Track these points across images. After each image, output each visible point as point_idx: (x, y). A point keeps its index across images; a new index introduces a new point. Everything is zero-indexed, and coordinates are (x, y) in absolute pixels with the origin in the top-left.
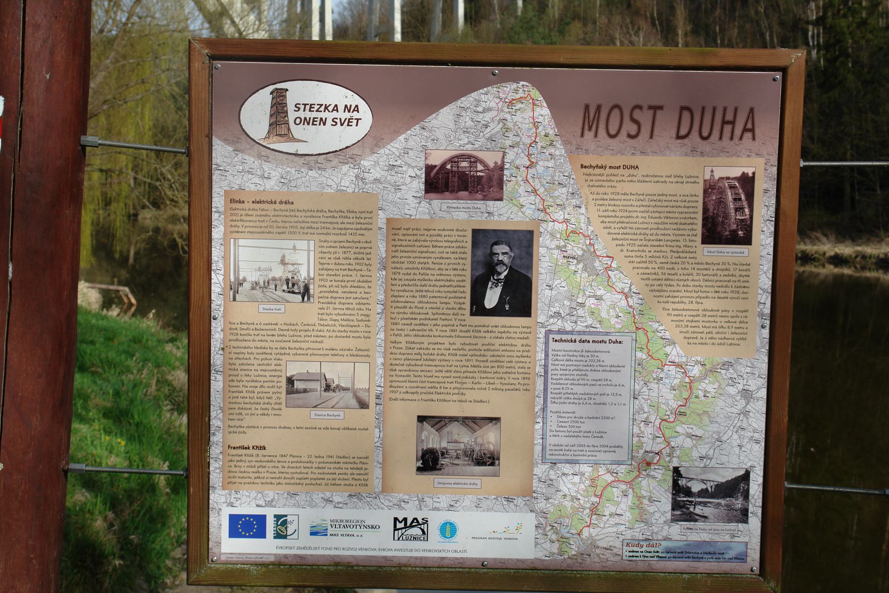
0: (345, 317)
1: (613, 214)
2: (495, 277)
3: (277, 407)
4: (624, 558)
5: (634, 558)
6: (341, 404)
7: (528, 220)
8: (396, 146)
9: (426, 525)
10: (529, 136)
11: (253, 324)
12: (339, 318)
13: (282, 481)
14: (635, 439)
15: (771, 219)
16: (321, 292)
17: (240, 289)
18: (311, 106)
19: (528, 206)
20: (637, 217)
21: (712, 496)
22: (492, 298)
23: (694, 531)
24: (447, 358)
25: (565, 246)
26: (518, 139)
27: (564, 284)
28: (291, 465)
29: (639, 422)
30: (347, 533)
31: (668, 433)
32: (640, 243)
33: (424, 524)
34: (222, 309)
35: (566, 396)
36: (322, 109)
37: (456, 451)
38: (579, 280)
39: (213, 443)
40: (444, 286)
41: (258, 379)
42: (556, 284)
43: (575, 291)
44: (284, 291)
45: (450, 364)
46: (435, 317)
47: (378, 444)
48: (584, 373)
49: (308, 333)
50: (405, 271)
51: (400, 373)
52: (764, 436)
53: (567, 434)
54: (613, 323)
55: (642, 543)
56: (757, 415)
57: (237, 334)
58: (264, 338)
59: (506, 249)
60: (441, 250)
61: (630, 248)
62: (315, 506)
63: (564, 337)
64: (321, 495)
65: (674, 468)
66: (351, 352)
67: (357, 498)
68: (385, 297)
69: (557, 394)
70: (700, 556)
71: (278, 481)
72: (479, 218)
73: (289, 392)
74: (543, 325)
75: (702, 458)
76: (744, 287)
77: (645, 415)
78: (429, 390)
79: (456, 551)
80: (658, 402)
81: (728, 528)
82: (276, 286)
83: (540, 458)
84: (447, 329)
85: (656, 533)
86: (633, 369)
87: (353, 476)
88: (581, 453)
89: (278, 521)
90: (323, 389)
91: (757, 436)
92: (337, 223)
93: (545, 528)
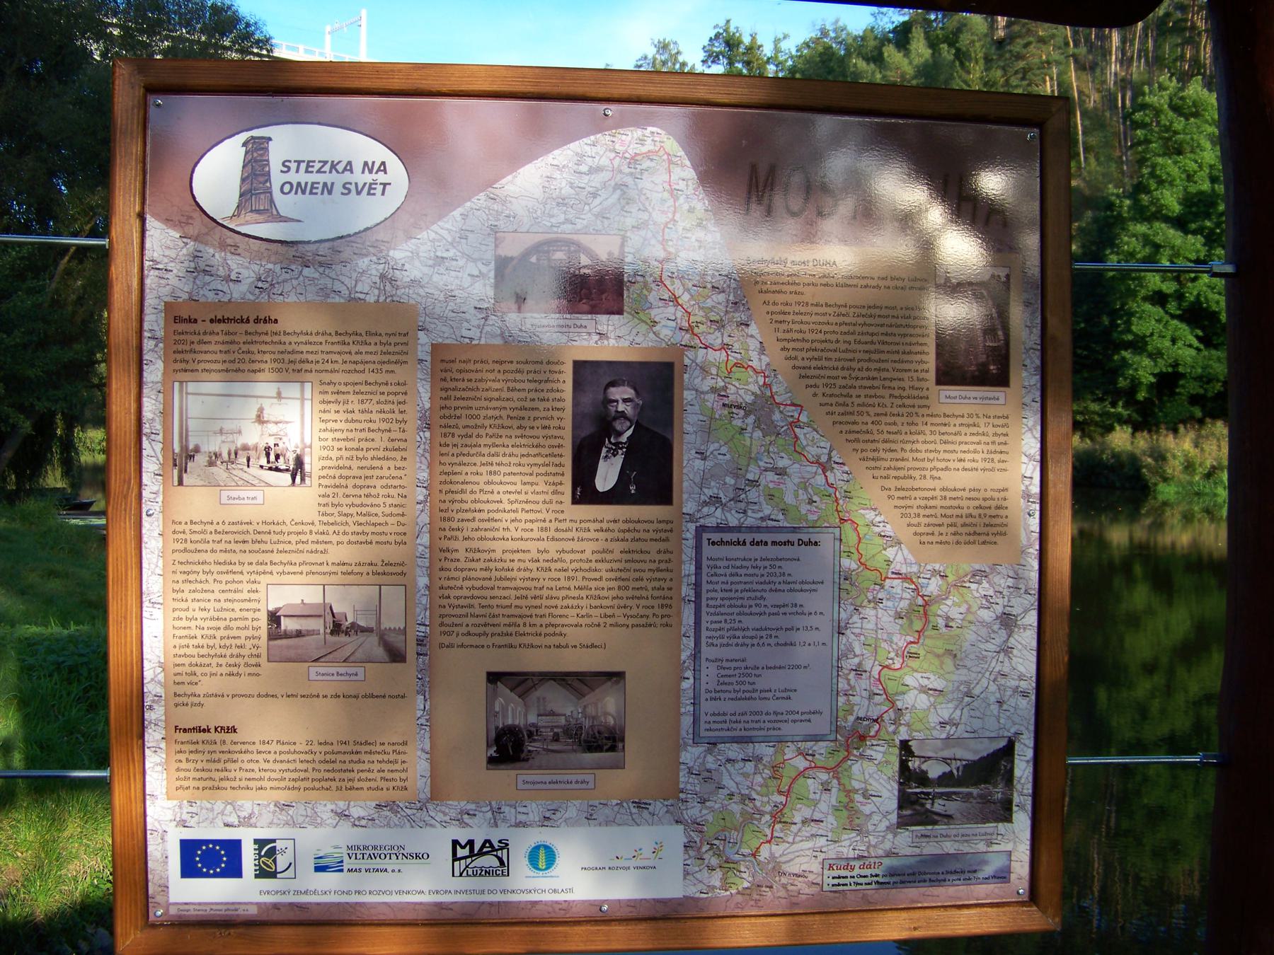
0: (364, 510)
1: (800, 336)
2: (613, 440)
3: (253, 661)
4: (826, 888)
5: (841, 888)
6: (359, 655)
7: (664, 345)
8: (447, 226)
9: (505, 851)
10: (663, 212)
11: (212, 523)
12: (353, 510)
13: (265, 784)
14: (842, 699)
15: (1035, 347)
16: (323, 468)
17: (189, 464)
18: (309, 164)
19: (664, 322)
20: (838, 341)
21: (959, 782)
22: (607, 475)
23: (932, 839)
24: (535, 574)
25: (725, 388)
26: (645, 216)
27: (724, 450)
28: (278, 758)
29: (846, 672)
30: (376, 867)
31: (892, 688)
32: (843, 382)
33: (502, 849)
34: (160, 499)
35: (731, 632)
36: (327, 168)
37: (552, 730)
38: (748, 443)
39: (150, 722)
40: (528, 455)
41: (222, 614)
42: (711, 449)
43: (743, 462)
44: (262, 467)
45: (539, 585)
46: (514, 506)
47: (423, 721)
48: (758, 594)
49: (303, 538)
50: (463, 432)
51: (456, 602)
52: (1034, 685)
53: (733, 695)
54: (803, 512)
55: (852, 863)
56: (1025, 652)
57: (186, 540)
58: (229, 547)
59: (628, 392)
60: (522, 395)
61: (828, 391)
62: (321, 824)
63: (727, 537)
64: (330, 806)
65: (901, 742)
66: (375, 569)
67: (391, 810)
68: (430, 474)
69: (714, 630)
70: (941, 877)
71: (259, 784)
72: (585, 343)
73: (272, 636)
74: (692, 518)
75: (943, 724)
76: (1001, 452)
77: (856, 660)
78: (505, 630)
79: (555, 891)
80: (876, 639)
81: (983, 831)
82: (248, 460)
83: (691, 736)
84: (535, 526)
85: (875, 847)
86: (837, 586)
87: (382, 774)
88: (756, 725)
89: (260, 849)
90: (328, 631)
91: (1023, 685)
92: (350, 353)
93: (701, 847)
